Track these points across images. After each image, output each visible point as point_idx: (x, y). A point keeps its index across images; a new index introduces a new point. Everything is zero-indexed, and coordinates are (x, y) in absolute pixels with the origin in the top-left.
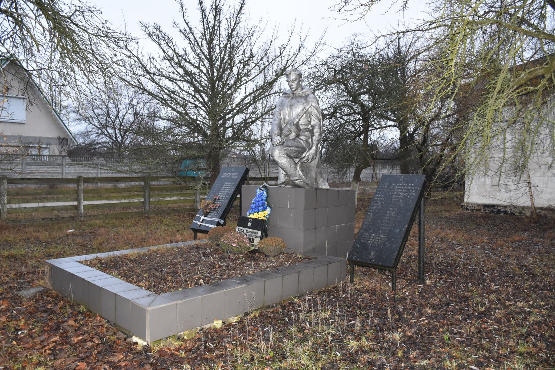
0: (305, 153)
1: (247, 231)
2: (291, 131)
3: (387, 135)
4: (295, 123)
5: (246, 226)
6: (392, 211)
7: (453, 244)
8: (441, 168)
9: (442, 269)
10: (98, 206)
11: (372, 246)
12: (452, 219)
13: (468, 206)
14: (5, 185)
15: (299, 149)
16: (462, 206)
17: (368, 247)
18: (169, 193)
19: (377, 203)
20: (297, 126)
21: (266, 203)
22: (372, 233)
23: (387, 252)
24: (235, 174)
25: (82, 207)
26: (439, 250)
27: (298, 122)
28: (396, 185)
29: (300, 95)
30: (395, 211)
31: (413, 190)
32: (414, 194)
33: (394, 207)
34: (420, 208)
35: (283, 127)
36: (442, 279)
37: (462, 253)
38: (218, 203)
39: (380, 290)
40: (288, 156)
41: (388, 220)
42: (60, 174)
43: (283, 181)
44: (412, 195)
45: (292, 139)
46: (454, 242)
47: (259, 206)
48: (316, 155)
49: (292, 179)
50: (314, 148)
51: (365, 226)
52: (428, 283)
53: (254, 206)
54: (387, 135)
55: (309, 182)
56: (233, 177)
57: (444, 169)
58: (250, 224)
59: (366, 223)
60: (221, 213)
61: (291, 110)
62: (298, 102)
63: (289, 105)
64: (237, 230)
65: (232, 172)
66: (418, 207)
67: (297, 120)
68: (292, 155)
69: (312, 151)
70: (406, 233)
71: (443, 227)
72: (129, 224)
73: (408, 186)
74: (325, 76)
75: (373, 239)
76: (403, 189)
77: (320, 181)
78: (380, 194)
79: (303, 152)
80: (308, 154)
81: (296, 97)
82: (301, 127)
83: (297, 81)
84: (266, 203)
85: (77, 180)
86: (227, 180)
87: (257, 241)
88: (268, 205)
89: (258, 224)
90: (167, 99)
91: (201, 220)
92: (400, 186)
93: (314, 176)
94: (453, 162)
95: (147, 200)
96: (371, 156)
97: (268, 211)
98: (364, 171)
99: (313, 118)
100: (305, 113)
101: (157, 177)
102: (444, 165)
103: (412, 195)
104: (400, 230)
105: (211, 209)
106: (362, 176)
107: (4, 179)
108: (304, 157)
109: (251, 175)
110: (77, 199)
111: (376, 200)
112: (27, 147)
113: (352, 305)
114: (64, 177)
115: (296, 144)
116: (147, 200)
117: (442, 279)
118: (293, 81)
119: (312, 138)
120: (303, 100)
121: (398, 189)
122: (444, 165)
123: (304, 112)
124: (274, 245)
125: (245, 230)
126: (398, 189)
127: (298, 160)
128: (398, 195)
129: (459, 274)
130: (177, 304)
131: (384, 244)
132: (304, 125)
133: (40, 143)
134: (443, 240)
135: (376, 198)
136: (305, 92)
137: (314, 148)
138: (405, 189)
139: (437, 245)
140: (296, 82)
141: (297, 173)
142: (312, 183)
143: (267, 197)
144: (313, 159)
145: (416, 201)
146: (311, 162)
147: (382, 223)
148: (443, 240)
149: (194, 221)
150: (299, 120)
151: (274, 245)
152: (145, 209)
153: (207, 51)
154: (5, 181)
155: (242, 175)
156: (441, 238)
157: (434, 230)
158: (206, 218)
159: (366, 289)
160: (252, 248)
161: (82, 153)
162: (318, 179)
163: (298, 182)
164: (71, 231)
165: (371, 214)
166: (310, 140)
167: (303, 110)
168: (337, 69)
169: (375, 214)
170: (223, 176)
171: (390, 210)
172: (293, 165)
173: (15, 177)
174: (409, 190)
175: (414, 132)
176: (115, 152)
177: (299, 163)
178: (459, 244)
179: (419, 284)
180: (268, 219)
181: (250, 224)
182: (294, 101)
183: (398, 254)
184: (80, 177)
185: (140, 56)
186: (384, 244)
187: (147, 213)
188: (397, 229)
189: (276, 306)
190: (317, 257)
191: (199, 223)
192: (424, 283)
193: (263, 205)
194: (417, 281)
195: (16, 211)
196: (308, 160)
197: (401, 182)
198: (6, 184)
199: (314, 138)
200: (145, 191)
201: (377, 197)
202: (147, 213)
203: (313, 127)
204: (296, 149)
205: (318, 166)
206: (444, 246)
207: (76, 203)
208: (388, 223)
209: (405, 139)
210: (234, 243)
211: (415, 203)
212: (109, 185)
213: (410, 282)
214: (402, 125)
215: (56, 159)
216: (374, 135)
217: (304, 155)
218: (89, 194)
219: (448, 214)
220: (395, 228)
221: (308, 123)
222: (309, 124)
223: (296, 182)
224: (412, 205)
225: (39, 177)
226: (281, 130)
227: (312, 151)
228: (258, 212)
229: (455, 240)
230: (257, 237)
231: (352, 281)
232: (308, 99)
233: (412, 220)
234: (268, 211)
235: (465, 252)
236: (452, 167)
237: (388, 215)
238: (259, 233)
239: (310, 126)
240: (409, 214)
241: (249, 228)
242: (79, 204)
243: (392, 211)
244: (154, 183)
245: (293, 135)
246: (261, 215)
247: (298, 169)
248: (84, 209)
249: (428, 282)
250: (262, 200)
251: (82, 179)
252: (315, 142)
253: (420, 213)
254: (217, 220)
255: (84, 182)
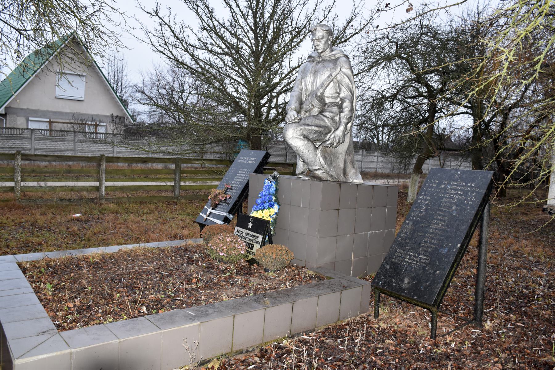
0: (329, 135)
2: (313, 105)
3: (458, 123)
4: (319, 94)
5: (246, 228)
6: (441, 220)
7: (529, 260)
8: (518, 162)
9: (511, 303)
10: (122, 188)
11: (406, 270)
12: (530, 225)
13: (551, 210)
14: (19, 162)
15: (320, 129)
16: (544, 210)
19: (421, 208)
20: (321, 99)
21: (274, 198)
22: (409, 250)
23: (427, 282)
24: (253, 159)
25: (103, 189)
26: (509, 269)
27: (322, 94)
28: (449, 183)
29: (328, 58)
30: (444, 221)
31: (473, 192)
32: (474, 200)
33: (443, 216)
34: (481, 218)
35: (304, 100)
36: (509, 320)
38: (229, 193)
39: (413, 335)
40: (306, 137)
41: (432, 233)
43: (302, 170)
44: (471, 200)
46: (531, 258)
47: (265, 202)
48: (344, 138)
50: (342, 128)
51: (400, 239)
52: (487, 328)
53: (259, 201)
54: (458, 123)
55: (333, 173)
56: (250, 162)
57: (522, 164)
58: (250, 225)
59: (402, 235)
60: (231, 206)
61: (315, 77)
62: (324, 67)
63: (313, 71)
64: (236, 231)
65: (250, 157)
66: (478, 218)
67: (321, 90)
68: (311, 137)
69: (339, 132)
70: (457, 257)
71: (518, 235)
72: (145, 211)
73: (466, 186)
74: (386, 51)
75: (408, 259)
76: (458, 190)
77: (351, 172)
78: (425, 195)
79: (327, 134)
80: (332, 136)
81: (324, 61)
82: (327, 101)
83: (325, 39)
84: (274, 198)
85: (130, 160)
86: (243, 165)
87: (257, 247)
88: (277, 201)
89: (260, 226)
90: (203, 74)
91: (208, 213)
92: (455, 185)
93: (342, 165)
94: (536, 153)
96: (441, 145)
97: (276, 209)
99: (343, 89)
100: (332, 80)
101: (189, 159)
102: (523, 158)
103: (471, 200)
104: (449, 251)
106: (424, 167)
107: (18, 154)
108: (328, 140)
109: (272, 159)
110: (99, 180)
111: (419, 204)
112: (81, 125)
113: (363, 362)
114: (115, 155)
115: (317, 122)
116: (177, 184)
117: (509, 320)
118: (319, 40)
119: (340, 115)
120: (331, 65)
122: (523, 158)
123: (330, 80)
124: (274, 257)
125: (245, 231)
126: (452, 189)
128: (451, 198)
129: (537, 315)
130: (71, 353)
131: (424, 268)
133: (96, 122)
134: (516, 255)
135: (419, 201)
136: (334, 55)
137: (342, 128)
138: (461, 190)
139: (508, 261)
140: (323, 41)
141: (318, 161)
142: (338, 175)
143: (277, 190)
145: (476, 209)
147: (424, 237)
148: (516, 255)
149: (201, 214)
150: (324, 91)
151: (274, 257)
152: (175, 194)
153: (253, 21)
154: (19, 157)
155: (260, 160)
156: (514, 251)
157: (505, 239)
158: (214, 211)
159: (394, 331)
160: (251, 257)
161: (133, 131)
162: (348, 170)
163: (319, 173)
164: (78, 215)
165: (411, 223)
166: (337, 118)
167: (329, 77)
168: (400, 42)
169: (416, 223)
170: (239, 161)
171: (437, 219)
172: (312, 150)
173: (66, 154)
174: (467, 192)
175: (490, 121)
176: (179, 131)
177: (321, 147)
178: (538, 263)
179: (474, 328)
180: (275, 220)
181: (250, 225)
182: (320, 66)
185: (172, 24)
186: (424, 268)
187: (177, 198)
188: (445, 248)
189: (253, 350)
191: (205, 217)
192: (482, 327)
193: (270, 200)
195: (31, 189)
196: (332, 144)
197: (456, 181)
198: (20, 160)
199: (342, 115)
200: (175, 174)
202: (177, 198)
204: (317, 129)
205: (348, 152)
206: (517, 264)
207: (97, 184)
208: (432, 238)
209: (481, 130)
210: (222, 251)
211: (474, 212)
213: (461, 323)
214: (476, 110)
215: (23, 132)
216: (442, 124)
218: (112, 175)
219: (525, 218)
220: (442, 247)
221: (336, 95)
222: (338, 97)
223: (317, 172)
224: (470, 213)
226: (301, 103)
227: (339, 132)
228: (263, 210)
230: (257, 243)
231: (377, 315)
232: (338, 63)
233: (468, 236)
234: (276, 209)
235: (547, 275)
236: (535, 161)
237: (434, 226)
238: (260, 238)
239: (339, 99)
240: (465, 228)
241: (249, 229)
242: (101, 184)
243: (441, 220)
244: (185, 165)
245: (316, 111)
246: (266, 214)
247: (319, 155)
248: (105, 191)
249: (488, 325)
250: (270, 194)
251: (104, 157)
252: (344, 121)
253: (481, 227)
254: (225, 214)
255: (106, 162)
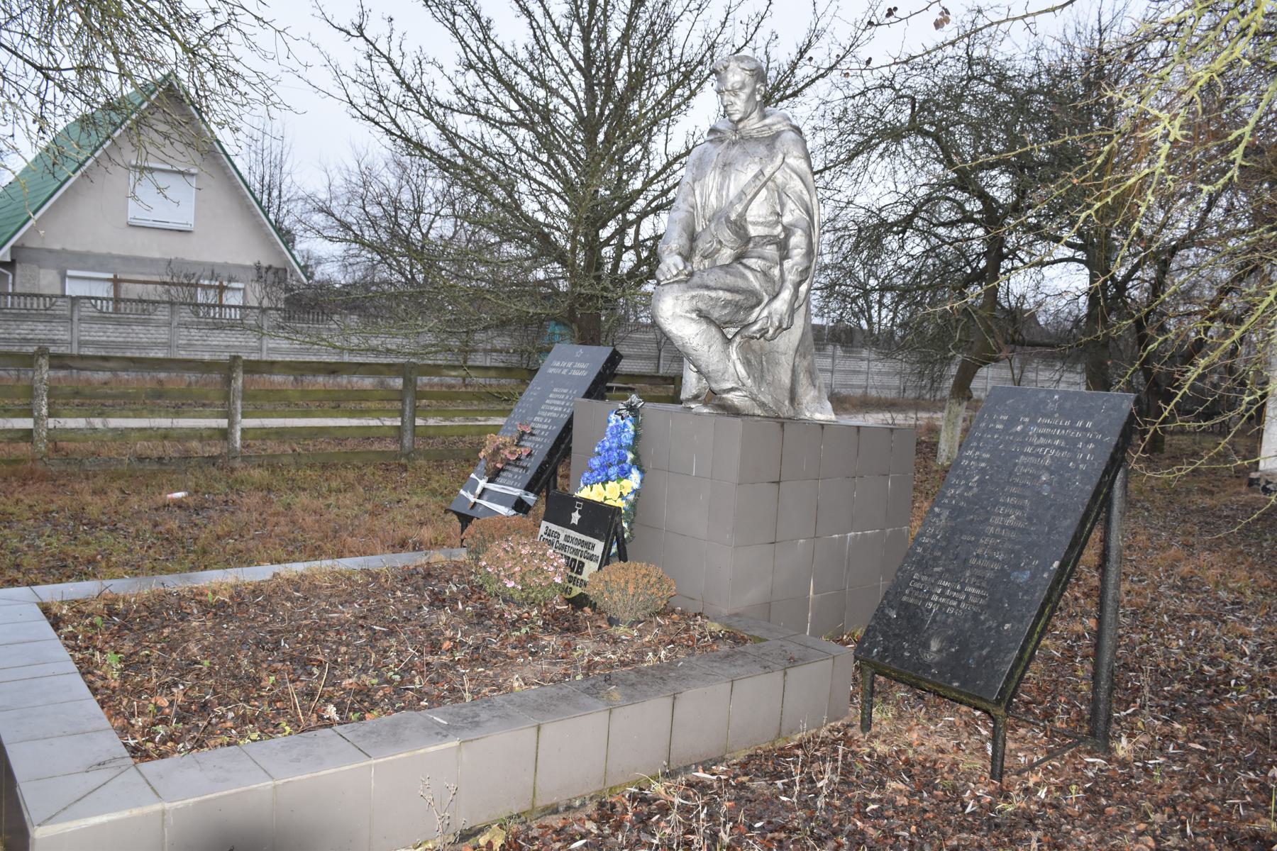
0: (757, 310)
1: (567, 538)
3: (1054, 283)
4: (733, 217)
5: (566, 523)
6: (1014, 506)
7: (1217, 599)
8: (1193, 374)
9: (1174, 696)
11: (934, 620)
13: (1268, 482)
14: (45, 373)
15: (737, 297)
16: (1252, 483)
17: (924, 621)
18: (484, 407)
19: (968, 478)
20: (739, 228)
21: (630, 456)
22: (940, 576)
23: (982, 648)
24: (583, 366)
25: (238, 434)
26: (1172, 618)
27: (742, 216)
28: (1033, 422)
29: (754, 134)
30: (1022, 508)
31: (1088, 442)
32: (1090, 460)
34: (1108, 502)
35: (699, 229)
36: (1171, 737)
37: (1244, 637)
38: (528, 444)
39: (951, 771)
40: (703, 316)
41: (994, 536)
42: (253, 350)
43: (695, 392)
44: (1084, 460)
45: (721, 267)
46: (1222, 594)
47: (610, 465)
48: (791, 316)
49: (715, 386)
50: (786, 295)
52: (1121, 753)
53: (596, 462)
54: (1054, 283)
55: (766, 399)
56: (575, 373)
57: (1201, 377)
58: (576, 517)
59: (925, 540)
60: (530, 473)
61: (724, 178)
62: (746, 153)
63: (720, 164)
64: (542, 530)
65: (575, 360)
66: (1101, 501)
67: (739, 208)
68: (716, 314)
69: (781, 304)
70: (1052, 590)
71: (1191, 540)
72: (334, 485)
73: (1072, 427)
74: (889, 117)
75: (942, 595)
76: (1053, 437)
77: (808, 395)
78: (978, 448)
79: (753, 307)
80: (765, 313)
81: (745, 139)
82: (753, 231)
83: (747, 91)
84: (630, 456)
86: (560, 381)
87: (590, 567)
88: (637, 463)
89: (599, 519)
90: (467, 170)
91: (478, 491)
92: (1047, 426)
93: (786, 380)
94: (1233, 353)
95: (408, 424)
96: (1015, 332)
97: (634, 480)
98: (983, 371)
99: (790, 205)
100: (765, 184)
101: (435, 366)
102: (1203, 362)
103: (1084, 460)
104: (1033, 577)
105: (508, 463)
106: (976, 384)
107: (42, 355)
108: (755, 322)
109: (625, 366)
110: (228, 415)
111: (964, 469)
112: (186, 288)
113: (835, 833)
114: (265, 357)
115: (730, 280)
116: (408, 424)
117: (1171, 737)
118: (734, 92)
119: (781, 265)
120: (762, 150)
121: (1039, 436)
122: (1203, 362)
123: (759, 184)
124: (631, 591)
125: (563, 532)
126: (1039, 436)
127: (733, 330)
128: (1038, 456)
129: (1236, 725)
130: (163, 812)
131: (975, 616)
132: (762, 224)
133: (220, 279)
134: (1186, 586)
136: (769, 127)
137: (786, 295)
138: (1060, 437)
139: (1169, 601)
141: (731, 370)
142: (777, 401)
143: (636, 437)
144: (780, 329)
145: (1095, 480)
146: (773, 339)
147: (975, 544)
148: (1186, 586)
149: (462, 492)
150: (746, 208)
151: (631, 591)
153: (582, 49)
154: (44, 362)
155: (599, 368)
156: (1183, 578)
157: (1162, 548)
158: (491, 486)
159: (907, 762)
160: (577, 591)
161: (306, 302)
162: (801, 390)
163: (735, 398)
164: (179, 495)
166: (776, 271)
167: (756, 177)
168: (920, 97)
169: (956, 512)
170: (551, 371)
171: (1005, 504)
172: (717, 345)
173: (152, 355)
174: (1075, 441)
176: (411, 302)
177: (738, 339)
179: (1090, 754)
180: (633, 505)
181: (576, 517)
182: (735, 151)
183: (1020, 658)
184: (235, 358)
185: (396, 56)
186: (975, 616)
187: (407, 456)
188: (1024, 569)
189: (583, 805)
190: (765, 635)
191: (472, 499)
192: (1108, 751)
193: (622, 460)
194: (1082, 740)
196: (763, 331)
197: (1050, 416)
199: (787, 264)
200: (402, 400)
201: (970, 459)
202: (407, 456)
203: (788, 231)
204: (728, 296)
205: (800, 350)
206: (1189, 607)
207: (224, 423)
208: (995, 548)
209: (1107, 299)
211: (1090, 488)
212: (368, 382)
213: (1061, 743)
214: (1096, 253)
216: (1018, 284)
217: (754, 315)
218: (258, 402)
219: (1208, 501)
221: (774, 218)
222: (777, 223)
223: (730, 396)
224: (1082, 489)
225: (207, 357)
226: (693, 237)
227: (781, 304)
228: (604, 483)
229: (1226, 588)
230: (591, 558)
231: (866, 724)
232: (778, 144)
233: (1078, 543)
234: (634, 480)
235: (1258, 634)
236: (1231, 370)
237: (998, 520)
238: (599, 547)
239: (780, 228)
240: (1069, 524)
241: (573, 527)
242: (231, 424)
243: (1014, 506)
244: (425, 379)
245: (726, 255)
246: (612, 493)
247: (734, 356)
248: (242, 438)
249: (1123, 747)
250: (620, 447)
252: (791, 278)
253: (1108, 521)
254: (517, 492)
255: (245, 372)
